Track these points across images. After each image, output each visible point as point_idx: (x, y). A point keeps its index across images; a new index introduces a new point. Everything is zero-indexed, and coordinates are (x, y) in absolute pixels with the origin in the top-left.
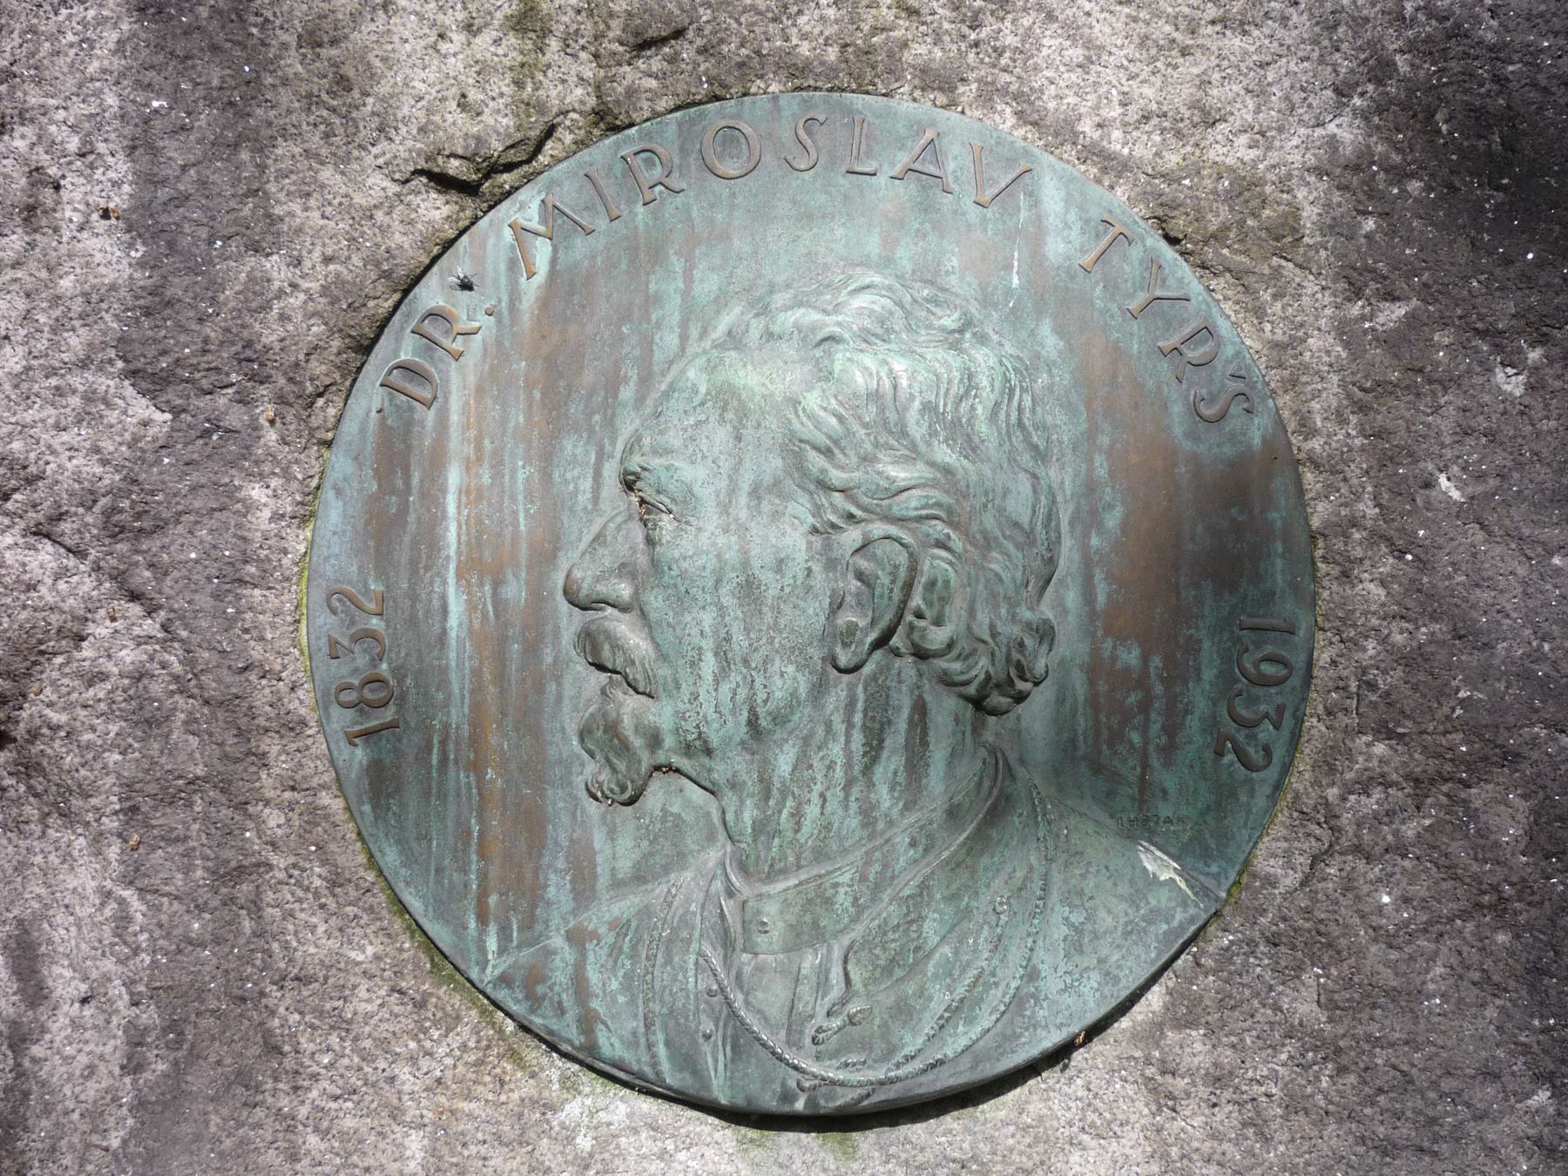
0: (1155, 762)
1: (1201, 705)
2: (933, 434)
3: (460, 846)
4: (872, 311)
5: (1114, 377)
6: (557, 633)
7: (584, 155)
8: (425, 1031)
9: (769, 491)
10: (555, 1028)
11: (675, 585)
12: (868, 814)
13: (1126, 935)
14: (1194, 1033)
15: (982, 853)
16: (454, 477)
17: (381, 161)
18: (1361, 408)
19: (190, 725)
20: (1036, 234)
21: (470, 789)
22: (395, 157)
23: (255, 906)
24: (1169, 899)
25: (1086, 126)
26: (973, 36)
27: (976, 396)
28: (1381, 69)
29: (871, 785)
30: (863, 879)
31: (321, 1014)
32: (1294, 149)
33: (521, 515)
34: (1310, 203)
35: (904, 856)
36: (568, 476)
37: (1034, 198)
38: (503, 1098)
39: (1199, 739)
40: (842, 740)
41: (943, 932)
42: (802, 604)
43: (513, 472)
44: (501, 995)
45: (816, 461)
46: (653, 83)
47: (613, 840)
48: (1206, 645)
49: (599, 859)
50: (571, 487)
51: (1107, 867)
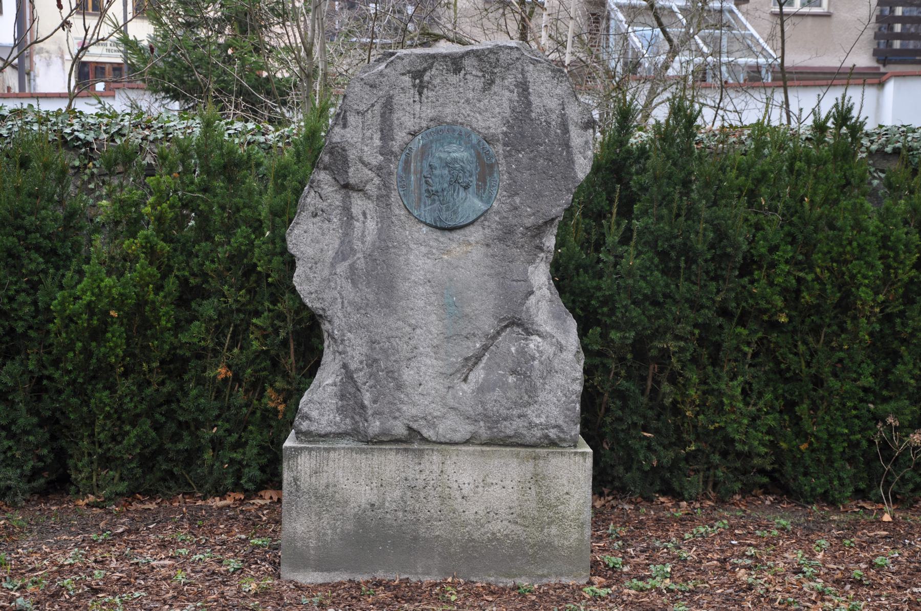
32: (499, 131)
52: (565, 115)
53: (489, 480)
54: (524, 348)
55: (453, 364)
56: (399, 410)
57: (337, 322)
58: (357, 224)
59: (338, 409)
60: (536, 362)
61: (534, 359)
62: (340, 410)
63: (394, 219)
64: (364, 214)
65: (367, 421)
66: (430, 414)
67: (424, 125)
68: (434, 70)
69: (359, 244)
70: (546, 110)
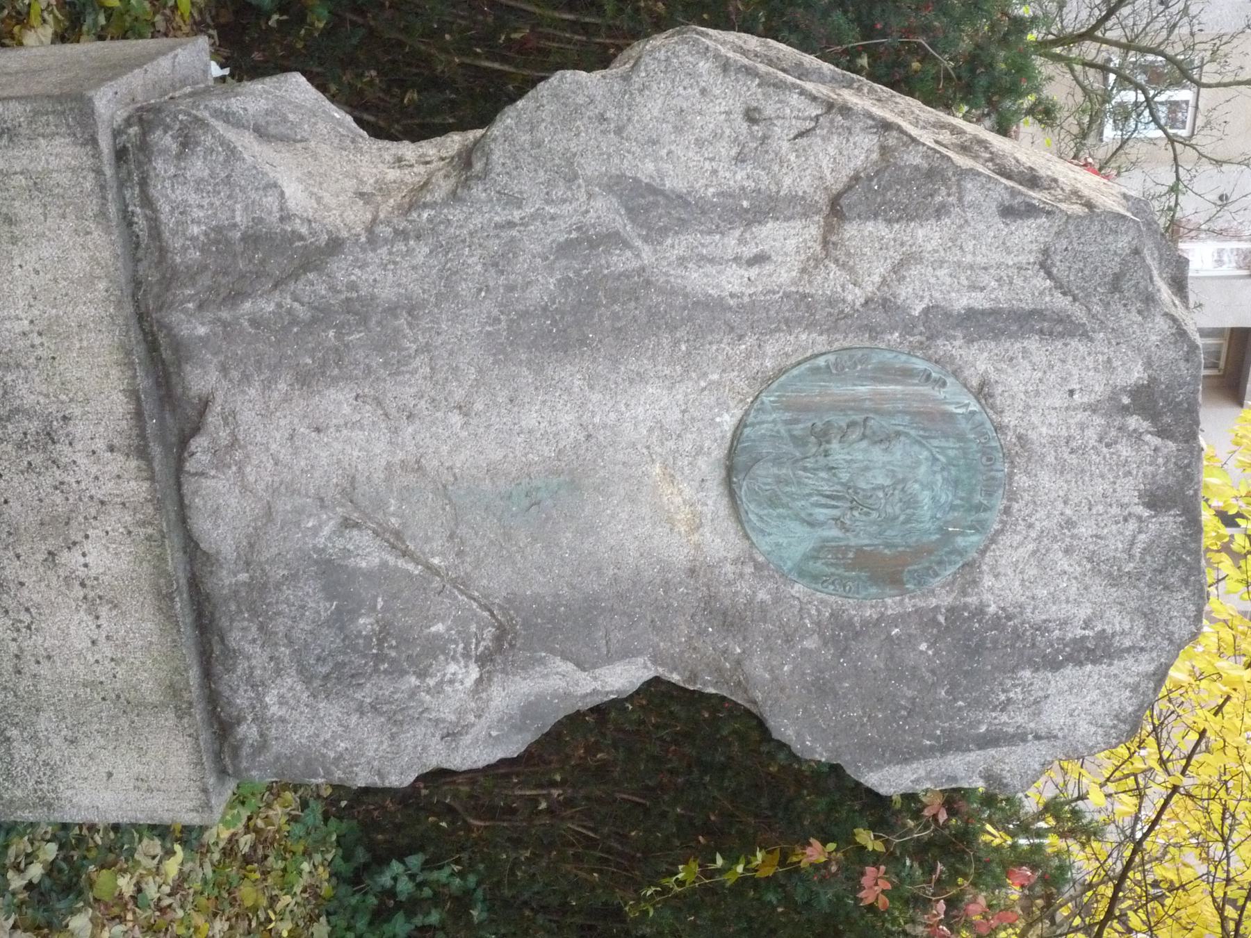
12: (810, 495)
16: (899, 388)
18: (916, 611)
19: (830, 314)
20: (962, 534)
23: (778, 330)
25: (994, 546)
28: (1009, 618)
32: (987, 597)
34: (972, 600)
44: (759, 401)
45: (900, 487)
52: (1024, 740)
53: (104, 611)
54: (444, 651)
55: (381, 504)
56: (246, 378)
57: (456, 214)
58: (731, 240)
59: (219, 229)
60: (414, 681)
61: (422, 675)
62: (218, 238)
63: (750, 340)
64: (759, 259)
65: (200, 307)
66: (248, 456)
67: (1009, 419)
68: (1156, 441)
69: (679, 251)
70: (1036, 702)
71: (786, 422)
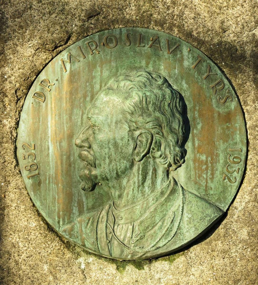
0: (209, 181)
1: (220, 169)
2: (155, 109)
3: (53, 201)
4: (142, 81)
5: (200, 93)
6: (74, 154)
7: (77, 43)
8: (47, 242)
9: (119, 122)
10: (75, 241)
11: (99, 143)
13: (200, 220)
14: (219, 242)
15: (169, 202)
17: (30, 45)
21: (55, 189)
22: (34, 45)
24: (211, 212)
25: (195, 33)
26: (167, 12)
27: (165, 100)
29: (144, 187)
30: (142, 207)
31: (24, 239)
33: (65, 127)
35: (151, 202)
36: (75, 118)
37: (181, 51)
38: (65, 257)
39: (219, 176)
40: (137, 177)
41: (160, 219)
42: (127, 147)
43: (63, 117)
46: (92, 26)
47: (87, 199)
48: (221, 155)
49: (84, 204)
50: (76, 120)
51: (197, 205)
71: (81, 212)
